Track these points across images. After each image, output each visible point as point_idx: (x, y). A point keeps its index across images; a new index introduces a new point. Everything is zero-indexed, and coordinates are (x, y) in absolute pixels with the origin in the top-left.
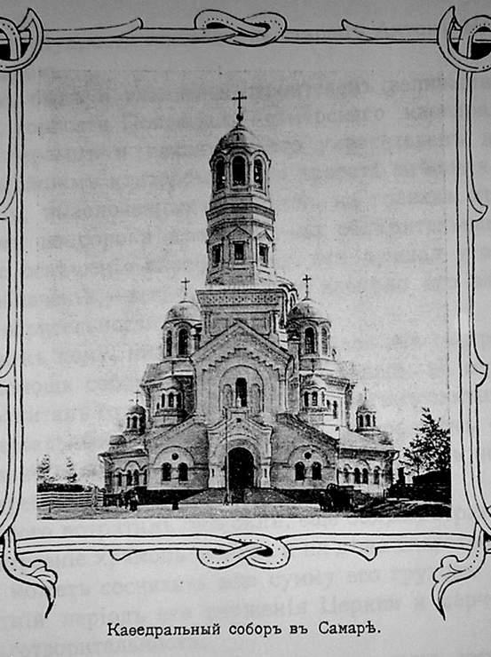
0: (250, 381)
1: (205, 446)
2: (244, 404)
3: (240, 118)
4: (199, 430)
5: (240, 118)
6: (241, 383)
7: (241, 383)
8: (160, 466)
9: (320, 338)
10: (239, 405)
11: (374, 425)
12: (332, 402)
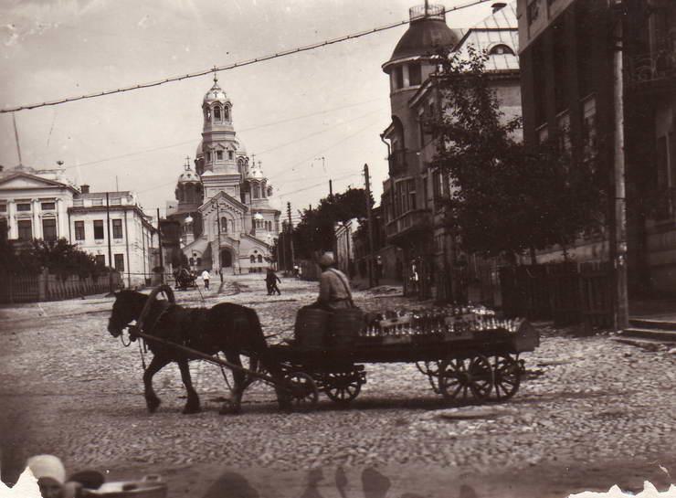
4: (207, 242)
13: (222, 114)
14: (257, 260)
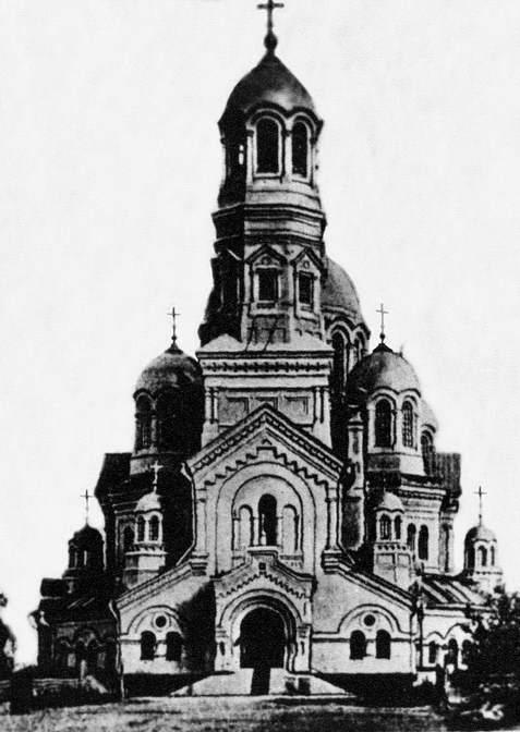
0: (283, 495)
1: (205, 600)
2: (272, 540)
3: (174, 338)
5: (174, 338)
6: (268, 503)
7: (268, 503)
8: (138, 637)
9: (400, 417)
10: (264, 540)
11: (493, 563)
12: (418, 529)
13: (286, 147)
14: (372, 649)
